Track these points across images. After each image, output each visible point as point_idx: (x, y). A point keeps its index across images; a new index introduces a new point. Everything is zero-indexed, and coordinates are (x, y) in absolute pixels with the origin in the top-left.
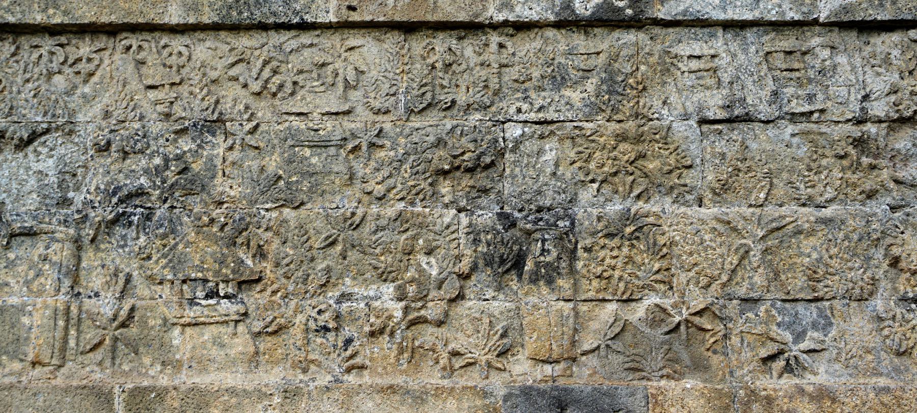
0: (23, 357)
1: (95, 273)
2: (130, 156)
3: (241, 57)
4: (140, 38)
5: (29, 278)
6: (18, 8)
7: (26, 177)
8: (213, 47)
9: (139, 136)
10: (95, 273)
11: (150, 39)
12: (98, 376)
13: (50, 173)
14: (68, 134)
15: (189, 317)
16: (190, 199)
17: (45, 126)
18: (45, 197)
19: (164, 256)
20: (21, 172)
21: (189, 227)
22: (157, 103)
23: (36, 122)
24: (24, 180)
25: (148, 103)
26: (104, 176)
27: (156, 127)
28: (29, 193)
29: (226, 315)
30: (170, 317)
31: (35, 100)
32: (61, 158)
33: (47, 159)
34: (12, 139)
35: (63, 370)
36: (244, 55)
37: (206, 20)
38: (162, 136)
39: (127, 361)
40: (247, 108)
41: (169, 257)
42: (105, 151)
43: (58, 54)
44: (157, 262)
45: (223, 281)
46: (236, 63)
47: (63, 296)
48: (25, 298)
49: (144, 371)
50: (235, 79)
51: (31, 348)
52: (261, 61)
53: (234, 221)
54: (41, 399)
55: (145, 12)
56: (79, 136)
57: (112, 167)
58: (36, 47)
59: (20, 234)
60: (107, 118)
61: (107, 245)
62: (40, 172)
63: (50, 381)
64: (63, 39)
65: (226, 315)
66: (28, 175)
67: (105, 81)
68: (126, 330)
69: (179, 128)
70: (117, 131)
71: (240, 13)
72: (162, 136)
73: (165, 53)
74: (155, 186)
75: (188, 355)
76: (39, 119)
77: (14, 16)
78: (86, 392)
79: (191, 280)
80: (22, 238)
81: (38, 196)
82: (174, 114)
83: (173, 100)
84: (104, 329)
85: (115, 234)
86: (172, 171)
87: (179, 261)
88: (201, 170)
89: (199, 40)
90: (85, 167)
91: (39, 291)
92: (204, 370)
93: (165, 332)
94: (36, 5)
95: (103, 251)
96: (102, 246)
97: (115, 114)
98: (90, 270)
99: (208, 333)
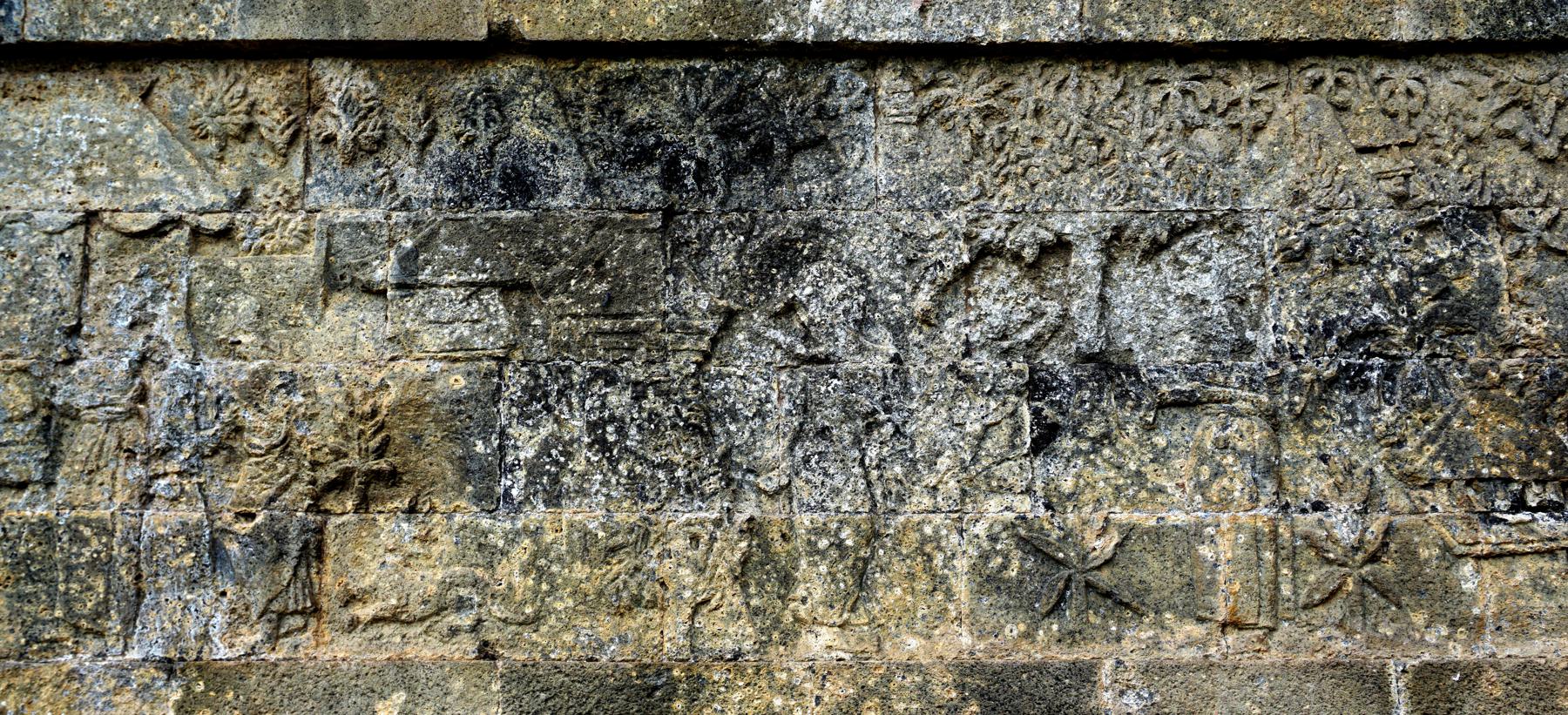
0: (1207, 615)
1: (1308, 470)
2: (1343, 268)
3: (1516, 98)
4: (1337, 66)
5: (1202, 478)
6: (1135, 15)
7: (1163, 306)
8: (1465, 79)
9: (1358, 233)
10: (1308, 470)
11: (1354, 68)
12: (1341, 646)
13: (1212, 299)
14: (1231, 232)
15: (1488, 543)
16: (1459, 342)
17: (1192, 217)
18: (1208, 339)
19: (1431, 439)
20: (1154, 297)
21: (1463, 390)
22: (1380, 176)
23: (1178, 210)
24: (1160, 311)
25: (1366, 178)
26: (1299, 303)
27: (1387, 219)
28: (1176, 333)
29: (1551, 540)
30: (1455, 543)
31: (1169, 174)
32: (1222, 273)
33: (1199, 275)
34: (1137, 240)
35: (1277, 636)
36: (1520, 94)
37: (1461, 33)
38: (1397, 233)
39: (1387, 619)
40: (1538, 185)
41: (1441, 441)
42: (1298, 260)
43: (1198, 93)
44: (1419, 450)
45: (1537, 482)
46: (1508, 107)
47: (1266, 510)
48: (1200, 514)
49: (1418, 636)
50: (1509, 135)
51: (1222, 599)
52: (1552, 102)
53: (1543, 379)
54: (1265, 686)
55: (1356, 21)
56: (1248, 234)
57: (1314, 287)
58: (1158, 82)
59: (1176, 404)
60: (1297, 204)
61: (1324, 421)
62: (1189, 297)
63: (1260, 655)
64: (1204, 69)
65: (1551, 540)
66: (1166, 303)
67: (1286, 139)
68: (1376, 566)
69: (1427, 219)
70: (1320, 225)
71: (1520, 22)
72: (1397, 233)
73: (1383, 90)
74: (1398, 320)
75: (1493, 609)
76: (1182, 205)
77: (1129, 30)
78: (1339, 673)
79: (1482, 480)
80: (1175, 411)
81: (1192, 338)
82: (1415, 196)
83: (1410, 172)
84: (1343, 565)
85: (1335, 403)
86: (1424, 294)
87: (1458, 448)
88: (1471, 291)
89: (1439, 69)
90: (1261, 287)
91: (1221, 500)
92: (1523, 634)
93: (1447, 568)
94: (1166, 10)
95: (1319, 431)
96: (1317, 424)
97: (1313, 196)
98: (1298, 464)
99: (1522, 571)
